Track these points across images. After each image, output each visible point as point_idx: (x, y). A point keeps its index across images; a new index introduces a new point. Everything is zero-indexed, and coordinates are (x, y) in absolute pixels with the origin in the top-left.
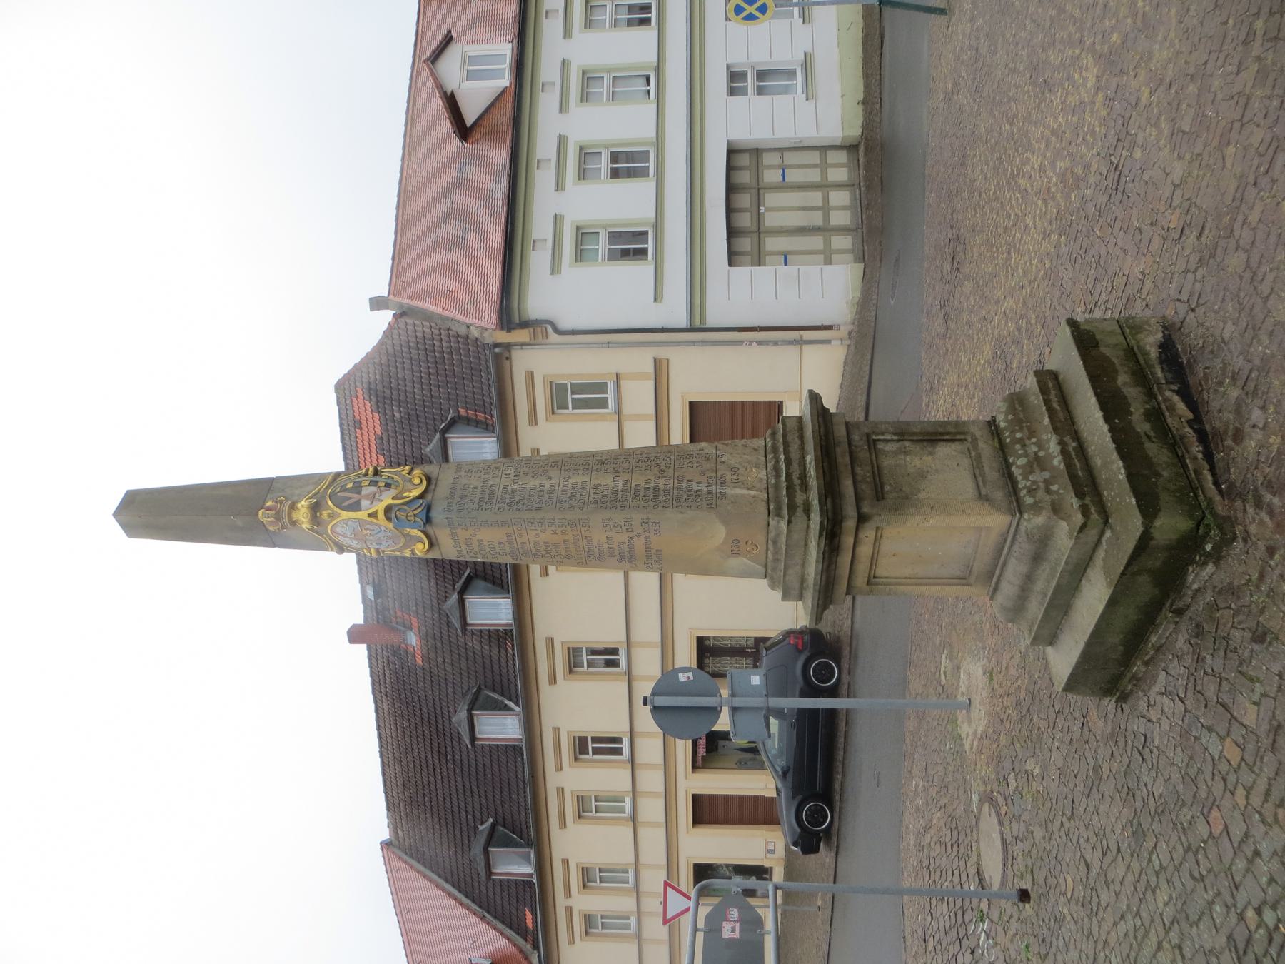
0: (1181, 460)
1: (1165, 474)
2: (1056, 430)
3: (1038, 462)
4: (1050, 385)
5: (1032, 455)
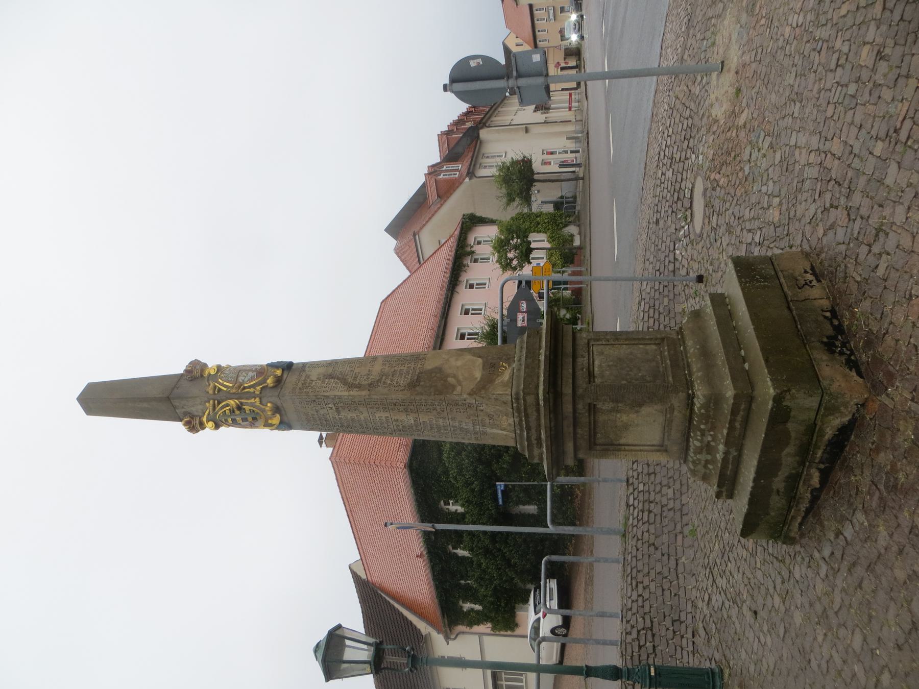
0: (789, 509)
1: (773, 514)
2: (727, 444)
3: (709, 448)
4: (743, 407)
5: (706, 443)
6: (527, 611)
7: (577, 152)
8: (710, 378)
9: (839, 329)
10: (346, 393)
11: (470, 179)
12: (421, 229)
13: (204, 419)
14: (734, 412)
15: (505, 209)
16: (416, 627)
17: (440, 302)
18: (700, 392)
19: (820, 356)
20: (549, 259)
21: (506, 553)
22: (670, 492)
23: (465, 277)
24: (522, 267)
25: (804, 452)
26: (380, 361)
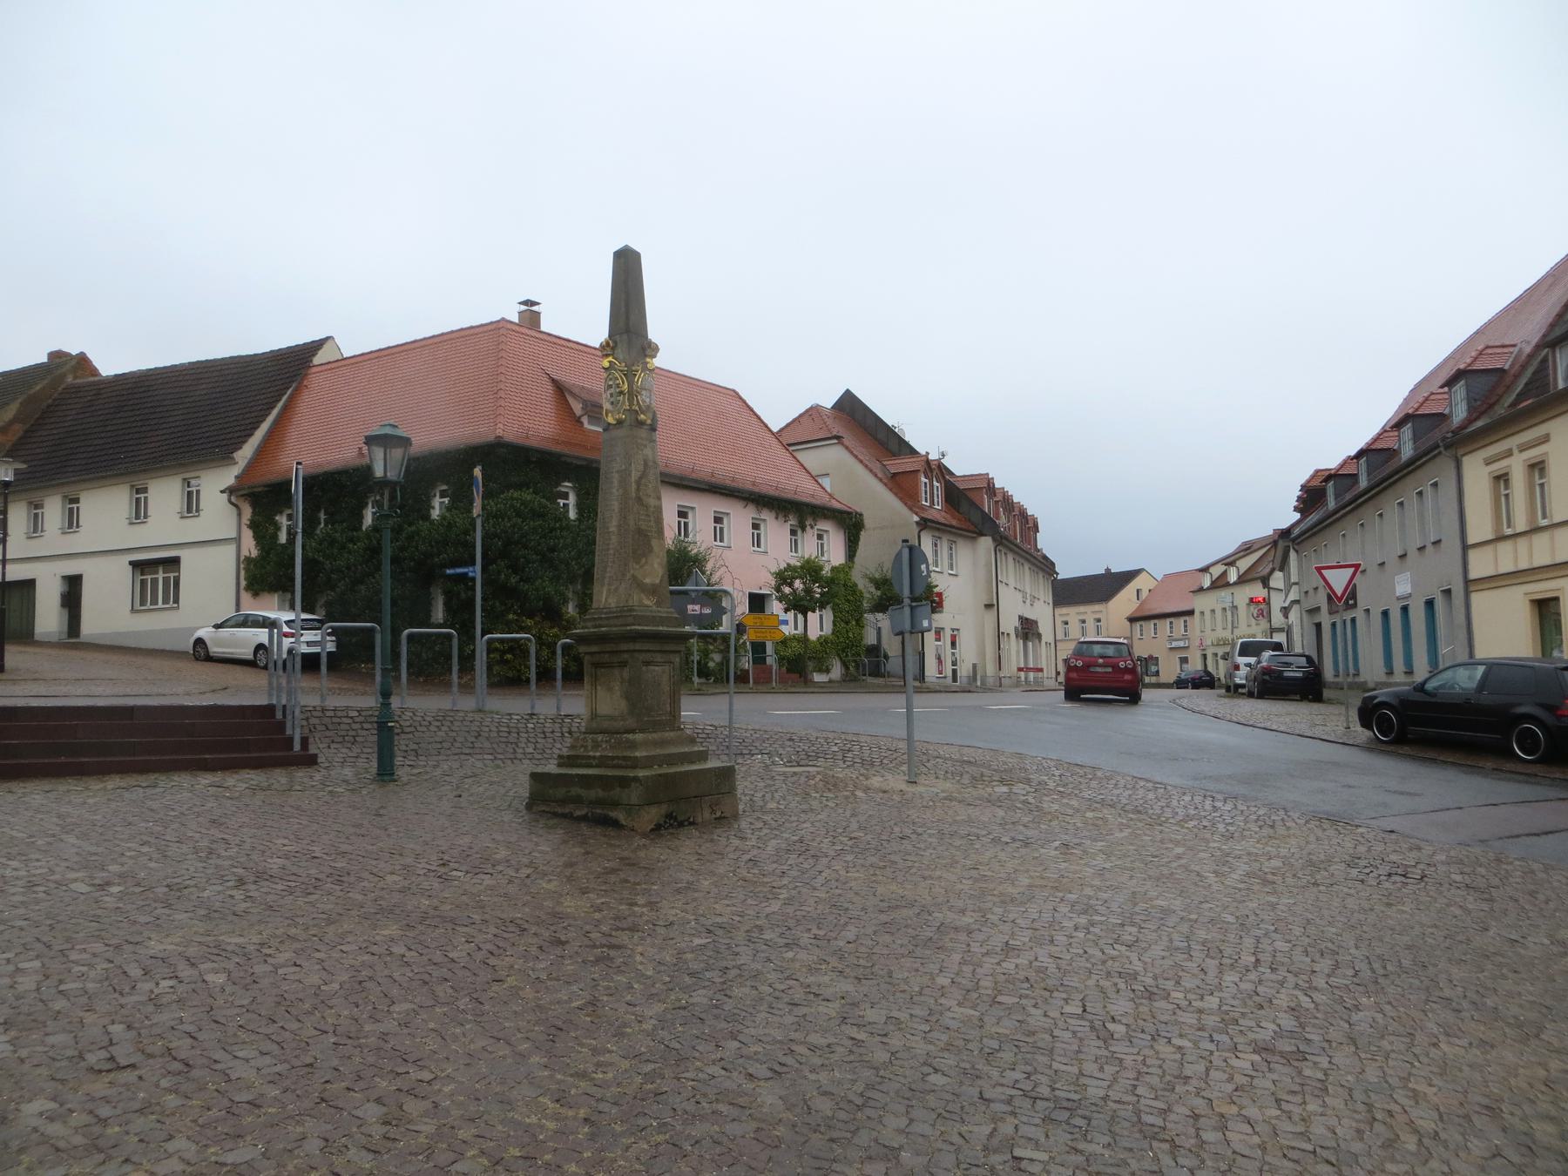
0: (557, 802)
1: (551, 791)
3: (596, 746)
6: (1441, 687)
7: (955, 679)
8: (646, 743)
9: (681, 825)
10: (633, 479)
11: (917, 523)
12: (847, 448)
13: (610, 359)
14: (624, 758)
15: (866, 576)
16: (244, 442)
17: (733, 481)
18: (639, 737)
19: (664, 809)
20: (794, 638)
21: (374, 578)
22: (531, 750)
23: (767, 515)
24: (780, 600)
25: (599, 802)
26: (657, 503)
